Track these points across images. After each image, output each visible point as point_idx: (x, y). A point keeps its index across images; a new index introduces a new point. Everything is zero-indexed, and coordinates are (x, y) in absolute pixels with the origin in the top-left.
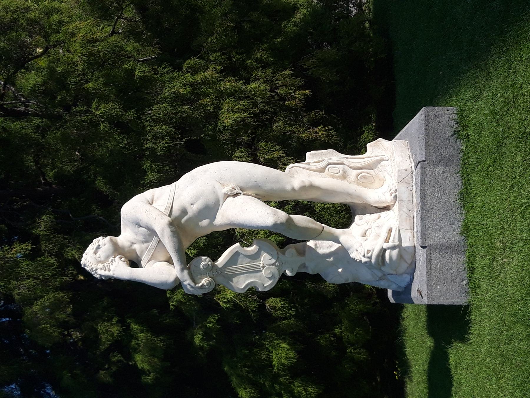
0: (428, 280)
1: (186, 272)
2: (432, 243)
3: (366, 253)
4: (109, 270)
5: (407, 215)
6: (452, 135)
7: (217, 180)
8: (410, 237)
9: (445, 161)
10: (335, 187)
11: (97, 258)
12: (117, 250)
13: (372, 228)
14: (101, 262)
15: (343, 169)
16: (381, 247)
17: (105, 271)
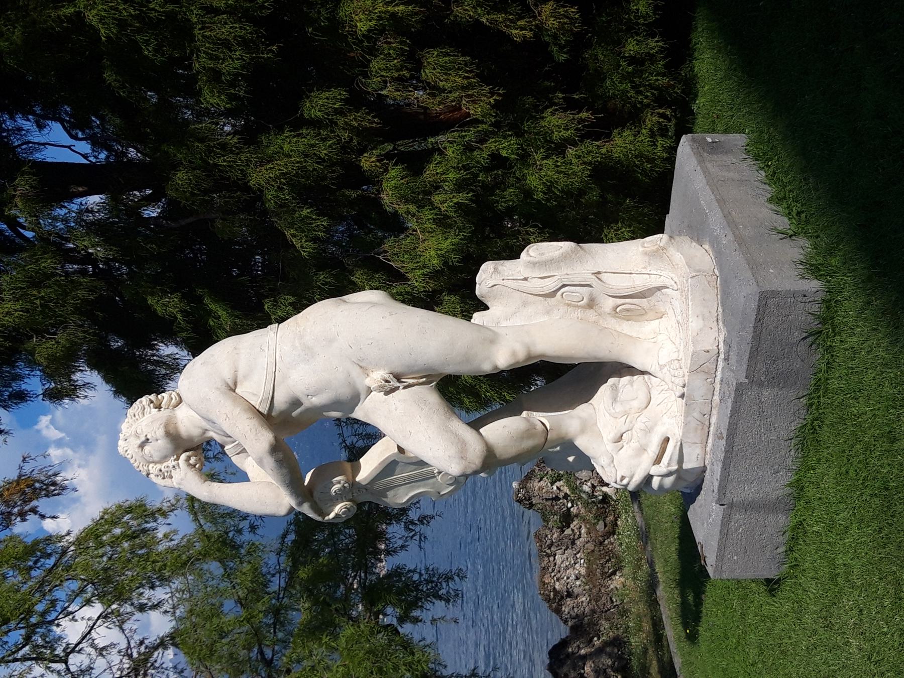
0: (720, 549)
2: (735, 499)
4: (171, 477)
5: (699, 423)
7: (353, 360)
8: (698, 455)
9: (780, 380)
10: (573, 352)
11: (147, 458)
13: (634, 429)
14: (155, 463)
15: (591, 295)
16: (646, 473)
17: (164, 478)
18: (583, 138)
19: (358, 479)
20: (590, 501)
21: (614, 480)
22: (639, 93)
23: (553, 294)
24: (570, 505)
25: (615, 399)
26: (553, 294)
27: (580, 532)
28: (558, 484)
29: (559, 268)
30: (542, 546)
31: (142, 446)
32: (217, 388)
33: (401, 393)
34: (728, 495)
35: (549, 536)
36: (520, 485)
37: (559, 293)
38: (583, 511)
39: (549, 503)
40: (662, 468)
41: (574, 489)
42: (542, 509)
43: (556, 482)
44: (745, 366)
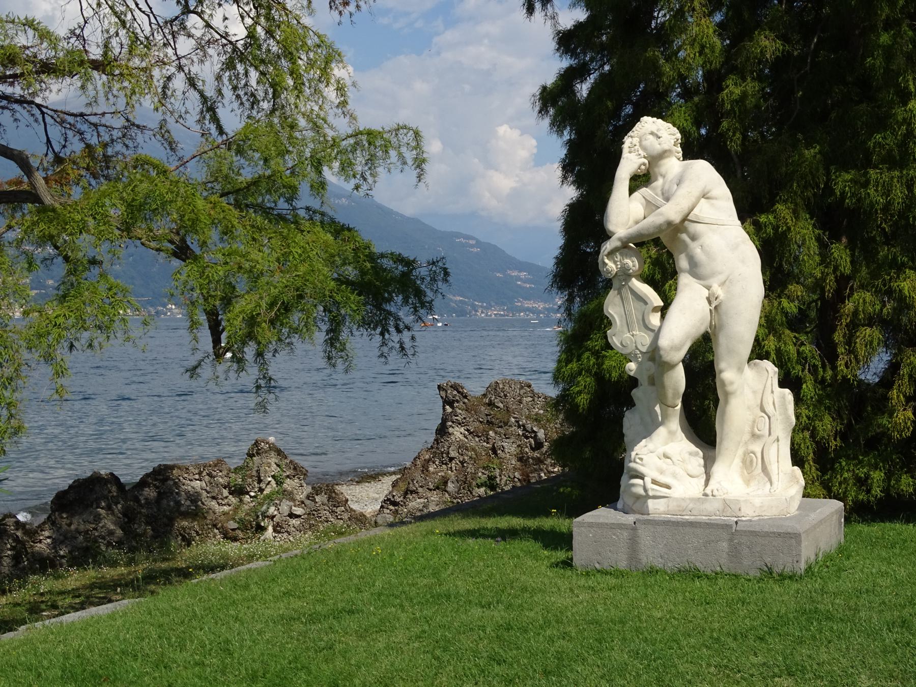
1: (618, 244)
3: (640, 456)
4: (630, 152)
6: (767, 566)
9: (735, 552)
12: (655, 159)
14: (640, 142)
18: (817, 443)
19: (634, 280)
20: (259, 513)
21: (639, 453)
22: (840, 484)
23: (763, 410)
24: (252, 494)
25: (690, 454)
26: (763, 410)
27: (225, 505)
28: (273, 482)
29: (780, 414)
30: (210, 466)
31: (652, 133)
32: (705, 187)
33: (707, 308)
34: (643, 526)
35: (220, 474)
36: (273, 444)
37: (764, 415)
38: (246, 507)
39: (254, 473)
40: (650, 485)
41: (269, 497)
42: (247, 466)
43: (275, 480)
44: (744, 529)
